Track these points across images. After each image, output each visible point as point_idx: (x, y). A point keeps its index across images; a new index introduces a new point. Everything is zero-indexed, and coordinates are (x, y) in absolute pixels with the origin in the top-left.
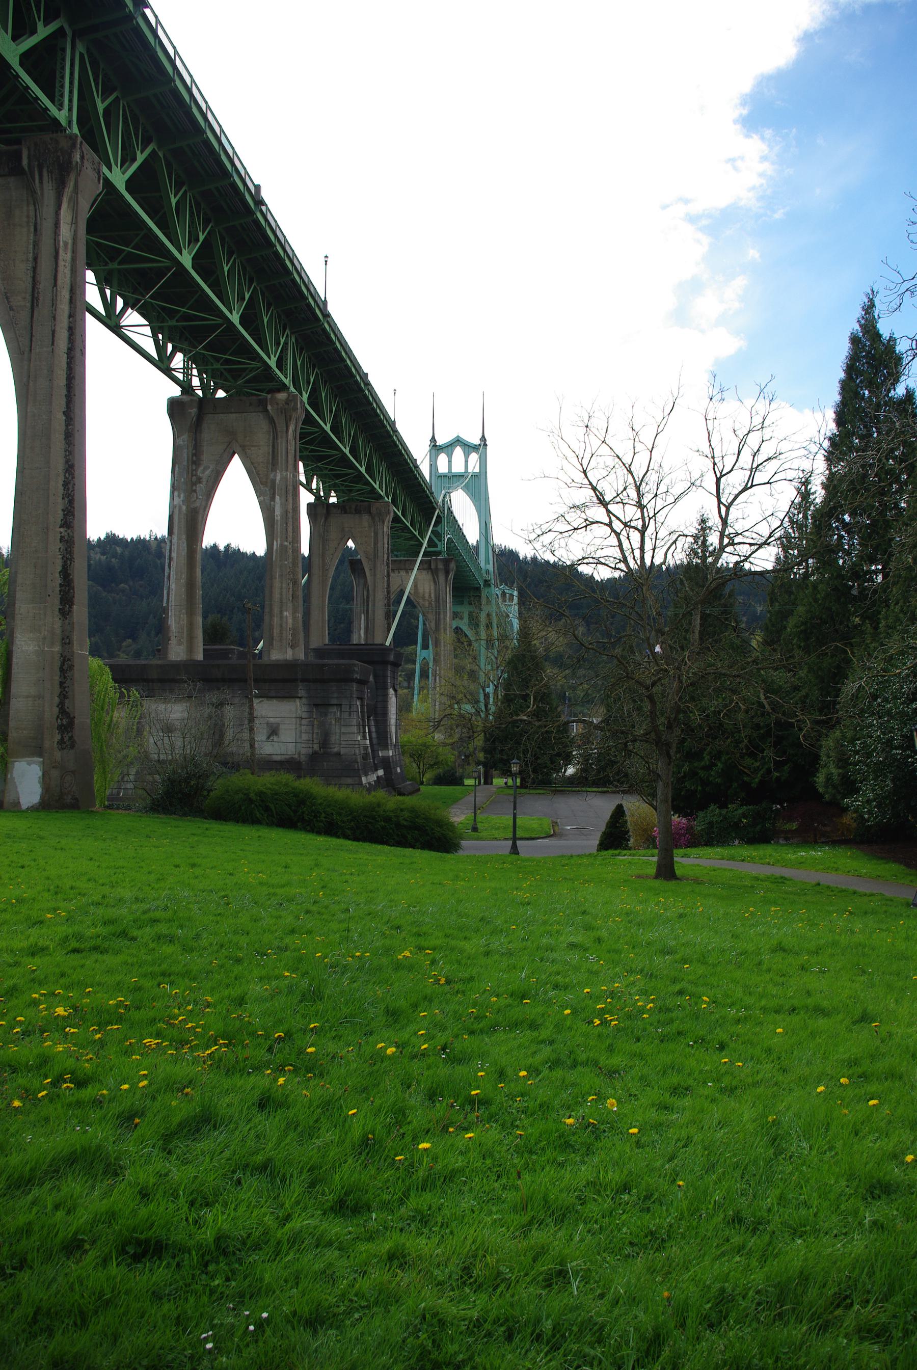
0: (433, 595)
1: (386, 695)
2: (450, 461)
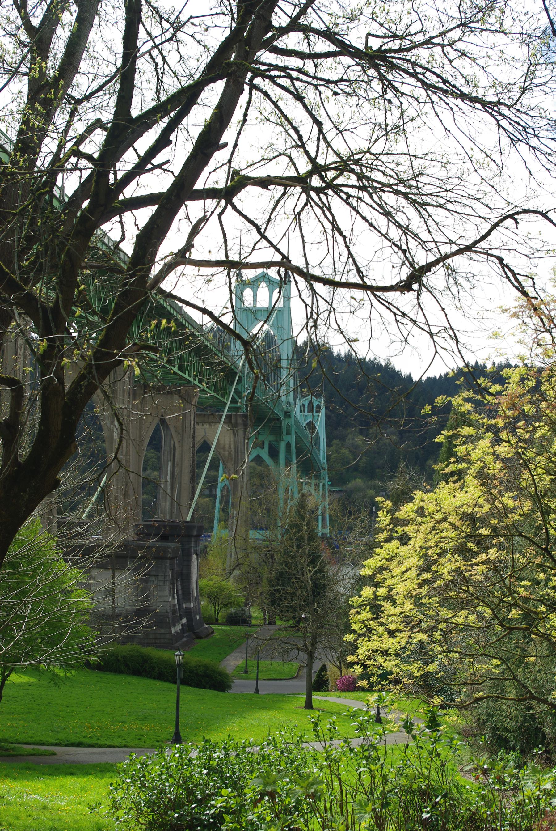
0: (232, 447)
1: (189, 561)
2: (255, 297)
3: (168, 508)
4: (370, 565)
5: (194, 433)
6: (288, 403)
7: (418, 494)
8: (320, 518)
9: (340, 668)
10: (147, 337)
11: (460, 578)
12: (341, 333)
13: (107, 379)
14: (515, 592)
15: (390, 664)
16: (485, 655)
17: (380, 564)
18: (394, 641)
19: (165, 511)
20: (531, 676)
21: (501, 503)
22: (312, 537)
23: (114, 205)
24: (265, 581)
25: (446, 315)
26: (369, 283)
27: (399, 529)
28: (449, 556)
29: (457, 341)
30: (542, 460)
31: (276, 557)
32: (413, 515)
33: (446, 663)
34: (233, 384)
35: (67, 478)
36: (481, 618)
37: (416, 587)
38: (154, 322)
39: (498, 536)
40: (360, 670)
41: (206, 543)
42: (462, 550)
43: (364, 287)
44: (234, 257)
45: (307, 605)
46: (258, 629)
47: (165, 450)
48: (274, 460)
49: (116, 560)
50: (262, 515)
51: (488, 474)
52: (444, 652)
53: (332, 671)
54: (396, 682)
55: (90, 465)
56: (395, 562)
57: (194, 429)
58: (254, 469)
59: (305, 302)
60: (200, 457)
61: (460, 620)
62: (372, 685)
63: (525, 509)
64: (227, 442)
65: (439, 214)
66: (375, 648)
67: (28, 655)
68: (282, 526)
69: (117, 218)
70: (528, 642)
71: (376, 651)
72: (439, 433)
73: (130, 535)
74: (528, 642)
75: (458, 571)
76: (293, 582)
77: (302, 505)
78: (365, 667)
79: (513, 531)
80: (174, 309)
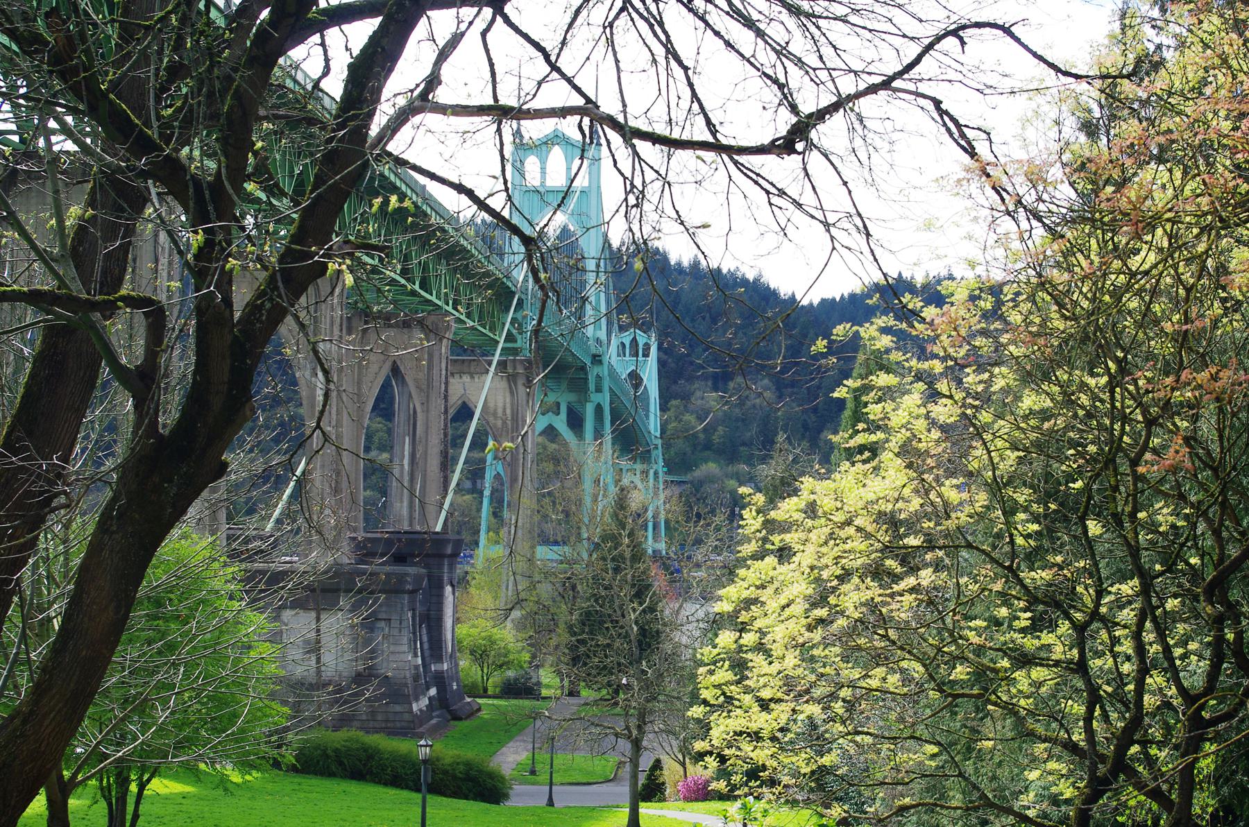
0: (508, 411)
2: (543, 171)
3: (405, 512)
4: (728, 598)
5: (446, 390)
6: (598, 340)
7: (807, 483)
8: (650, 525)
9: (683, 764)
10: (367, 232)
11: (875, 618)
12: (682, 223)
13: (303, 300)
14: (961, 637)
15: (762, 754)
16: (912, 737)
17: (745, 594)
18: (768, 717)
19: (401, 515)
20: (986, 769)
21: (940, 495)
22: (638, 556)
23: (310, 16)
24: (562, 626)
25: (850, 192)
26: (724, 141)
27: (776, 539)
28: (856, 580)
29: (868, 235)
30: (1003, 426)
31: (579, 588)
32: (799, 516)
33: (852, 752)
34: (508, 310)
35: (239, 462)
36: (907, 679)
37: (803, 630)
38: (377, 201)
39: (932, 548)
40: (715, 764)
41: (467, 568)
42: (877, 572)
43: (718, 147)
44: (508, 98)
45: (631, 663)
46: (552, 704)
47: (400, 418)
48: (575, 433)
49: (321, 594)
50: (558, 523)
51: (918, 450)
52: (849, 733)
53: (671, 772)
54: (773, 782)
55: (277, 440)
56: (770, 590)
57: (447, 383)
58: (545, 448)
59: (622, 174)
60: (456, 429)
61: (874, 683)
62: (734, 788)
63: (977, 505)
64: (500, 405)
65: (837, 31)
66: (739, 729)
67: (180, 746)
68: (589, 539)
69: (316, 38)
70: (982, 719)
71: (741, 733)
72: (840, 384)
73: (344, 556)
74: (982, 719)
75: (871, 605)
76: (607, 628)
77: (621, 503)
78: (723, 759)
79: (957, 542)
80: (412, 190)
